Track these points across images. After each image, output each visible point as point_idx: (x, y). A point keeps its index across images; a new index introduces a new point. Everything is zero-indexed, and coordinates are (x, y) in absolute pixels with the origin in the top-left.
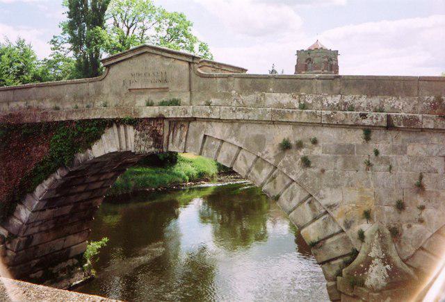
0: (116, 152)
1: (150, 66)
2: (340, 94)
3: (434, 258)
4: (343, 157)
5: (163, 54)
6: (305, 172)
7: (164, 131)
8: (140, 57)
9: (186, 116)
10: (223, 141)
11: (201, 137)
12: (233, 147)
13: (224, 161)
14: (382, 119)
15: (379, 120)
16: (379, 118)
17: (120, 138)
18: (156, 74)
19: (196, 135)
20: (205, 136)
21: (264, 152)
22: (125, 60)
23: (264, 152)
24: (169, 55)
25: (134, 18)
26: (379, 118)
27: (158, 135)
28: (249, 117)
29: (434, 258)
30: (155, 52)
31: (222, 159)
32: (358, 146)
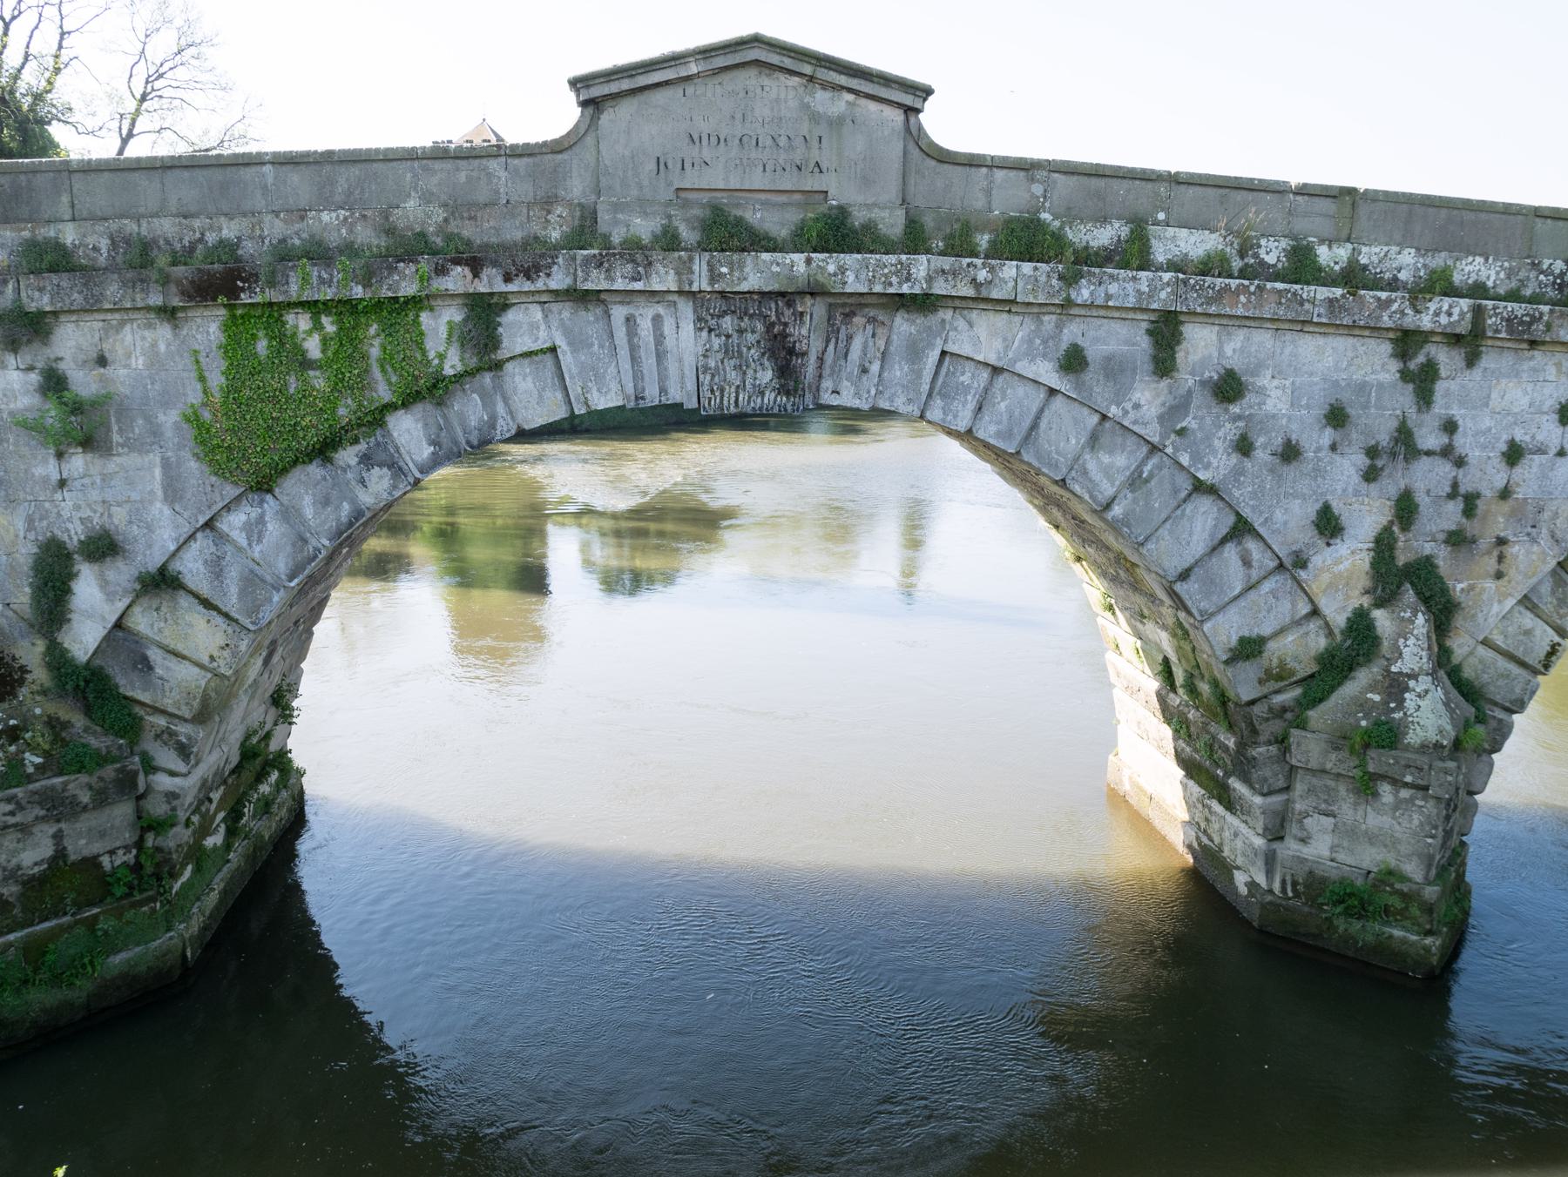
0: (622, 408)
1: (762, 110)
2: (1348, 240)
3: (1158, 880)
4: (357, 283)
5: (823, 74)
6: (1457, 474)
7: (808, 333)
8: (726, 77)
9: (905, 289)
10: (996, 371)
11: (934, 356)
12: (1030, 388)
13: (999, 434)
14: (1462, 314)
15: (1455, 317)
16: (1456, 311)
17: (634, 359)
18: (783, 141)
19: (914, 353)
20: (944, 353)
21: (1128, 406)
22: (667, 83)
23: (1128, 406)
24: (843, 80)
25: (1386, 255)
26: (1456, 311)
27: (791, 351)
28: (1109, 297)
29: (1158, 880)
30: (788, 63)
31: (993, 429)
32: (1380, 385)
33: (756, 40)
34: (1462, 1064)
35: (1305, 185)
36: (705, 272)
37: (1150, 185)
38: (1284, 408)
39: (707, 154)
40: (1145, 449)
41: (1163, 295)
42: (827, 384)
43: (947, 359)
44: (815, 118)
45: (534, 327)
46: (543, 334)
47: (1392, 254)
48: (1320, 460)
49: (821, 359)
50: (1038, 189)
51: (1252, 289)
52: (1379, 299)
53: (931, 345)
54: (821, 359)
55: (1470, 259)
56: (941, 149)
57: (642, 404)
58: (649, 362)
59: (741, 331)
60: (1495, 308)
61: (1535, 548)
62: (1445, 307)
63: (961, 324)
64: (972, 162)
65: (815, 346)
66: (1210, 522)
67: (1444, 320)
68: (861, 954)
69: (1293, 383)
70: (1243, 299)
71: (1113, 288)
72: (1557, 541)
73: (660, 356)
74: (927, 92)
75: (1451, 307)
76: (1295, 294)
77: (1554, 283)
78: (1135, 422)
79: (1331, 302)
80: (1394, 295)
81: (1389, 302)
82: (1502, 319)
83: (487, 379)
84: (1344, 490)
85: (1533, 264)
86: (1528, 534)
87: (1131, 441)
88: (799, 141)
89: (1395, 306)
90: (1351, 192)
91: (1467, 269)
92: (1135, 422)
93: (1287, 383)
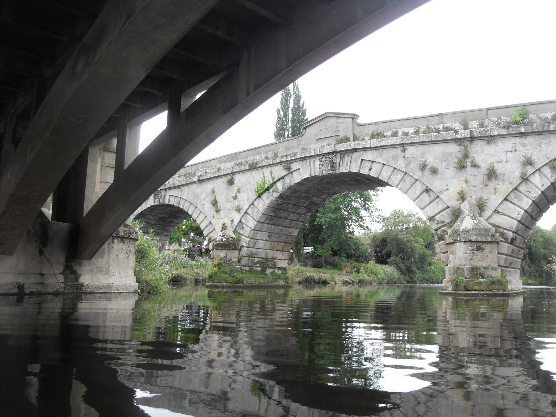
9: (350, 148)
14: (467, 133)
15: (466, 134)
16: (466, 133)
20: (362, 160)
21: (398, 165)
23: (398, 165)
28: (388, 143)
33: (327, 113)
34: (349, 331)
35: (430, 115)
36: (319, 151)
37: (399, 122)
38: (432, 160)
39: (321, 132)
40: (404, 173)
41: (399, 141)
42: (341, 168)
43: (363, 161)
44: (338, 123)
45: (297, 165)
46: (298, 166)
47: (453, 124)
48: (442, 170)
49: (339, 164)
50: (377, 127)
51: (417, 136)
52: (446, 133)
53: (359, 159)
54: (339, 164)
55: (472, 122)
56: (361, 124)
57: (311, 176)
58: (312, 168)
59: (325, 161)
60: (475, 130)
61: (505, 186)
62: (463, 132)
63: (364, 154)
64: (365, 125)
65: (338, 161)
66: (420, 188)
67: (463, 135)
68: (503, 308)
69: (434, 155)
70: (416, 139)
71: (389, 141)
72: (511, 183)
73: (314, 168)
74: (358, 116)
75: (464, 132)
76: (427, 136)
77: (496, 123)
78: (400, 168)
79: (435, 136)
80: (450, 132)
81: (449, 134)
82: (478, 132)
83: (290, 175)
84: (449, 177)
85: (489, 120)
86: (502, 183)
87: (400, 172)
88: (335, 128)
89: (450, 134)
90: (441, 114)
91: (472, 124)
92: (400, 168)
93: (432, 155)
